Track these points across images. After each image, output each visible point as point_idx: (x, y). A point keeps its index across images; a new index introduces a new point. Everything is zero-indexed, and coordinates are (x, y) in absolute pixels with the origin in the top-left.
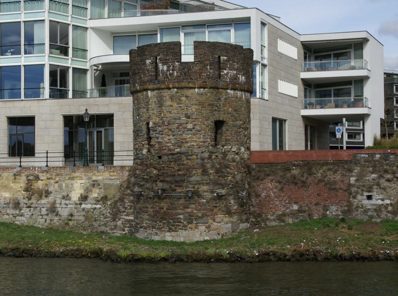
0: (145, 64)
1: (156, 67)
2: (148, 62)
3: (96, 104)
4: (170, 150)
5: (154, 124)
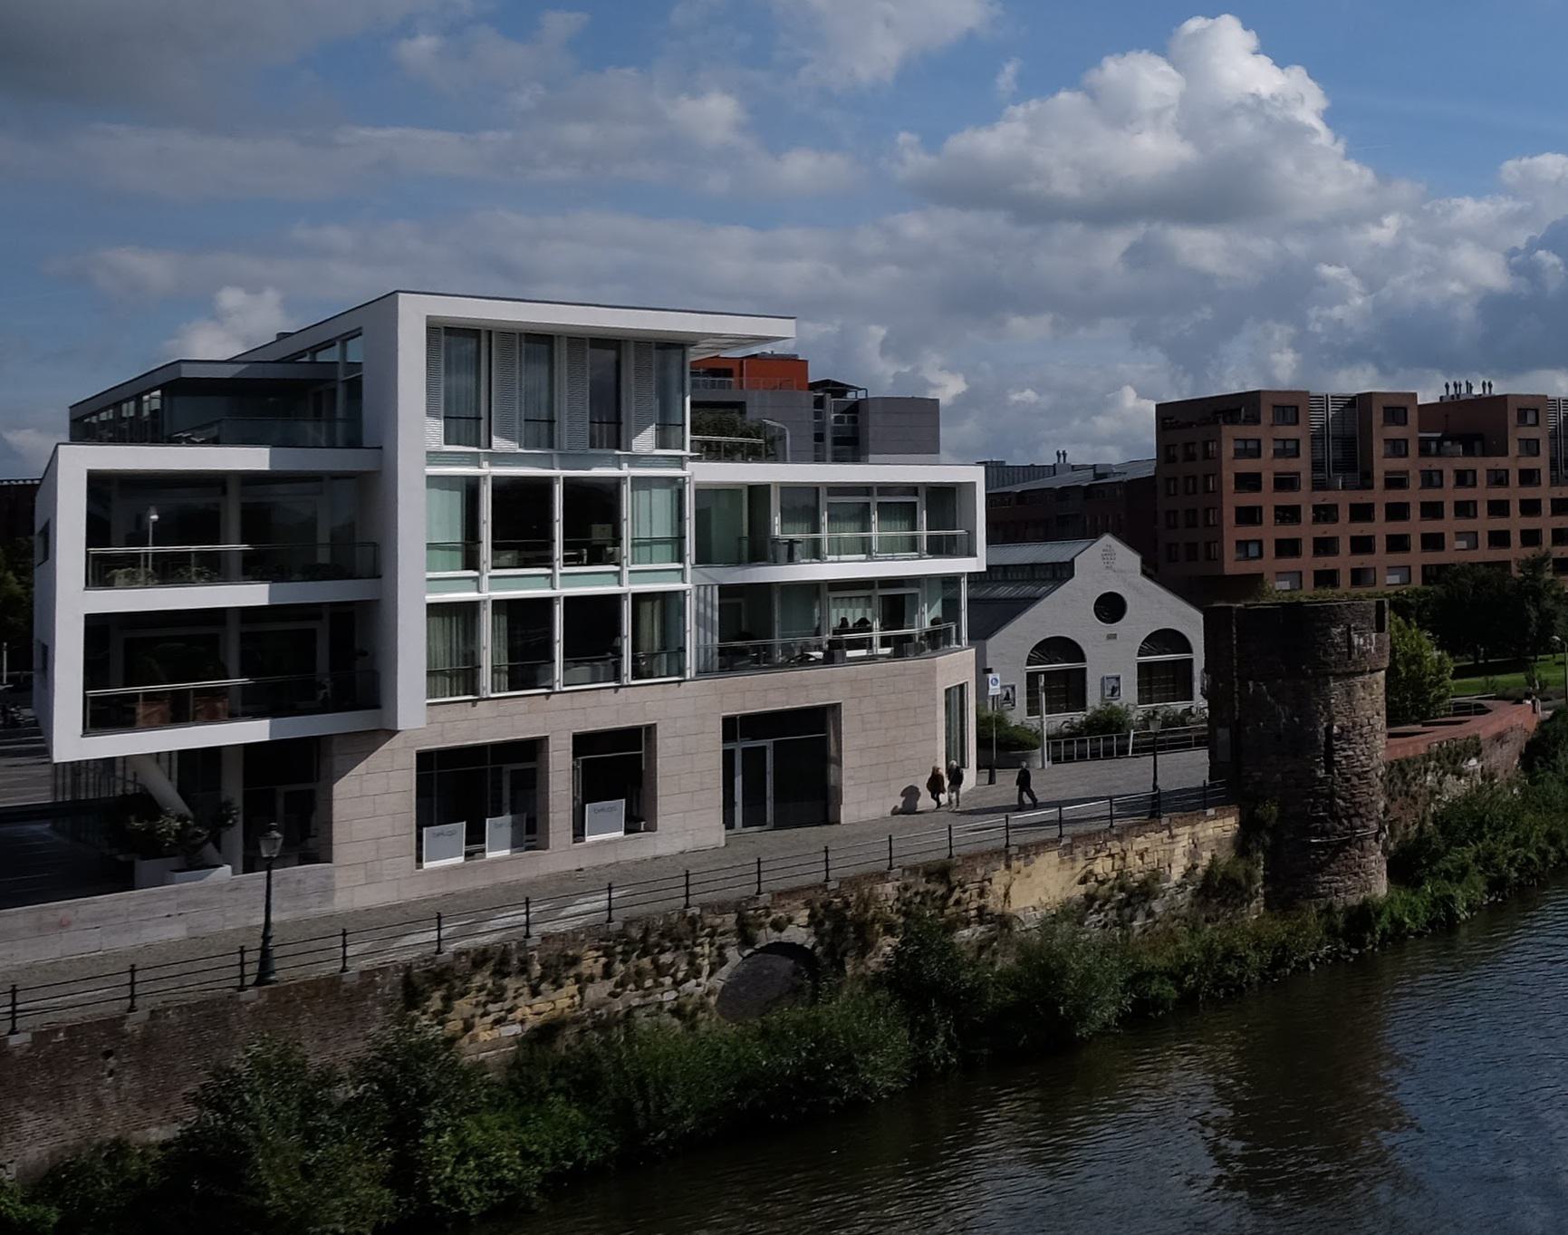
0: (1328, 635)
1: (1350, 640)
2: (1335, 631)
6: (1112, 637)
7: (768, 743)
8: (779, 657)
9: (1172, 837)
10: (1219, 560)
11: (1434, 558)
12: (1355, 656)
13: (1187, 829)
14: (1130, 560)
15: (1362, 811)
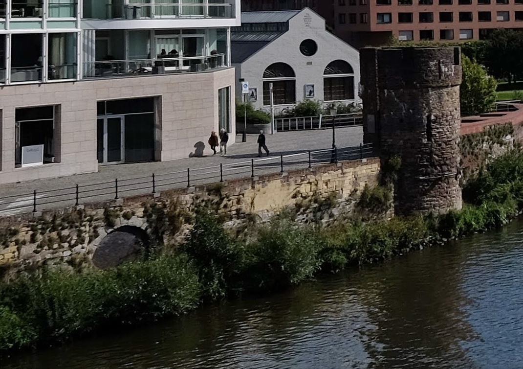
1: (440, 68)
3: (141, 84)
4: (448, 138)
5: (436, 116)
6: (310, 63)
7: (122, 116)
8: (128, 70)
9: (343, 173)
10: (368, 23)
11: (486, 25)
12: (443, 77)
13: (352, 170)
14: (320, 22)
15: (448, 162)
